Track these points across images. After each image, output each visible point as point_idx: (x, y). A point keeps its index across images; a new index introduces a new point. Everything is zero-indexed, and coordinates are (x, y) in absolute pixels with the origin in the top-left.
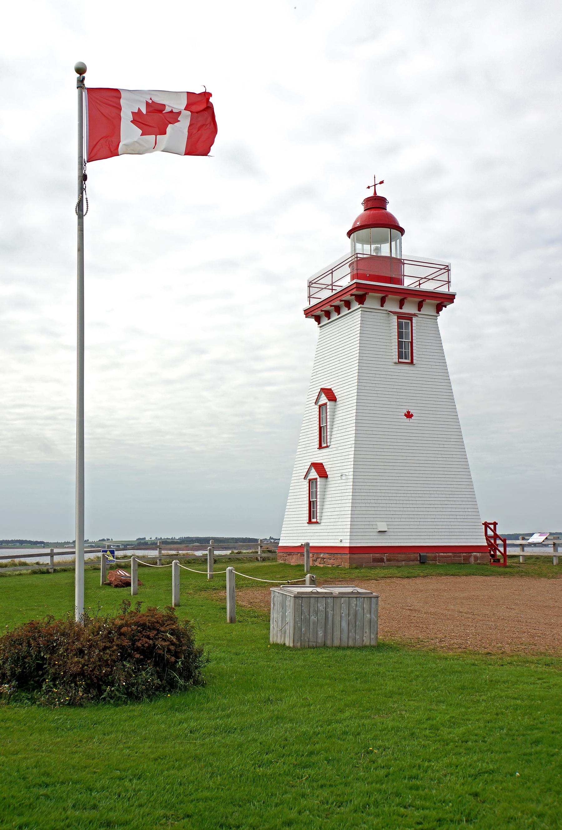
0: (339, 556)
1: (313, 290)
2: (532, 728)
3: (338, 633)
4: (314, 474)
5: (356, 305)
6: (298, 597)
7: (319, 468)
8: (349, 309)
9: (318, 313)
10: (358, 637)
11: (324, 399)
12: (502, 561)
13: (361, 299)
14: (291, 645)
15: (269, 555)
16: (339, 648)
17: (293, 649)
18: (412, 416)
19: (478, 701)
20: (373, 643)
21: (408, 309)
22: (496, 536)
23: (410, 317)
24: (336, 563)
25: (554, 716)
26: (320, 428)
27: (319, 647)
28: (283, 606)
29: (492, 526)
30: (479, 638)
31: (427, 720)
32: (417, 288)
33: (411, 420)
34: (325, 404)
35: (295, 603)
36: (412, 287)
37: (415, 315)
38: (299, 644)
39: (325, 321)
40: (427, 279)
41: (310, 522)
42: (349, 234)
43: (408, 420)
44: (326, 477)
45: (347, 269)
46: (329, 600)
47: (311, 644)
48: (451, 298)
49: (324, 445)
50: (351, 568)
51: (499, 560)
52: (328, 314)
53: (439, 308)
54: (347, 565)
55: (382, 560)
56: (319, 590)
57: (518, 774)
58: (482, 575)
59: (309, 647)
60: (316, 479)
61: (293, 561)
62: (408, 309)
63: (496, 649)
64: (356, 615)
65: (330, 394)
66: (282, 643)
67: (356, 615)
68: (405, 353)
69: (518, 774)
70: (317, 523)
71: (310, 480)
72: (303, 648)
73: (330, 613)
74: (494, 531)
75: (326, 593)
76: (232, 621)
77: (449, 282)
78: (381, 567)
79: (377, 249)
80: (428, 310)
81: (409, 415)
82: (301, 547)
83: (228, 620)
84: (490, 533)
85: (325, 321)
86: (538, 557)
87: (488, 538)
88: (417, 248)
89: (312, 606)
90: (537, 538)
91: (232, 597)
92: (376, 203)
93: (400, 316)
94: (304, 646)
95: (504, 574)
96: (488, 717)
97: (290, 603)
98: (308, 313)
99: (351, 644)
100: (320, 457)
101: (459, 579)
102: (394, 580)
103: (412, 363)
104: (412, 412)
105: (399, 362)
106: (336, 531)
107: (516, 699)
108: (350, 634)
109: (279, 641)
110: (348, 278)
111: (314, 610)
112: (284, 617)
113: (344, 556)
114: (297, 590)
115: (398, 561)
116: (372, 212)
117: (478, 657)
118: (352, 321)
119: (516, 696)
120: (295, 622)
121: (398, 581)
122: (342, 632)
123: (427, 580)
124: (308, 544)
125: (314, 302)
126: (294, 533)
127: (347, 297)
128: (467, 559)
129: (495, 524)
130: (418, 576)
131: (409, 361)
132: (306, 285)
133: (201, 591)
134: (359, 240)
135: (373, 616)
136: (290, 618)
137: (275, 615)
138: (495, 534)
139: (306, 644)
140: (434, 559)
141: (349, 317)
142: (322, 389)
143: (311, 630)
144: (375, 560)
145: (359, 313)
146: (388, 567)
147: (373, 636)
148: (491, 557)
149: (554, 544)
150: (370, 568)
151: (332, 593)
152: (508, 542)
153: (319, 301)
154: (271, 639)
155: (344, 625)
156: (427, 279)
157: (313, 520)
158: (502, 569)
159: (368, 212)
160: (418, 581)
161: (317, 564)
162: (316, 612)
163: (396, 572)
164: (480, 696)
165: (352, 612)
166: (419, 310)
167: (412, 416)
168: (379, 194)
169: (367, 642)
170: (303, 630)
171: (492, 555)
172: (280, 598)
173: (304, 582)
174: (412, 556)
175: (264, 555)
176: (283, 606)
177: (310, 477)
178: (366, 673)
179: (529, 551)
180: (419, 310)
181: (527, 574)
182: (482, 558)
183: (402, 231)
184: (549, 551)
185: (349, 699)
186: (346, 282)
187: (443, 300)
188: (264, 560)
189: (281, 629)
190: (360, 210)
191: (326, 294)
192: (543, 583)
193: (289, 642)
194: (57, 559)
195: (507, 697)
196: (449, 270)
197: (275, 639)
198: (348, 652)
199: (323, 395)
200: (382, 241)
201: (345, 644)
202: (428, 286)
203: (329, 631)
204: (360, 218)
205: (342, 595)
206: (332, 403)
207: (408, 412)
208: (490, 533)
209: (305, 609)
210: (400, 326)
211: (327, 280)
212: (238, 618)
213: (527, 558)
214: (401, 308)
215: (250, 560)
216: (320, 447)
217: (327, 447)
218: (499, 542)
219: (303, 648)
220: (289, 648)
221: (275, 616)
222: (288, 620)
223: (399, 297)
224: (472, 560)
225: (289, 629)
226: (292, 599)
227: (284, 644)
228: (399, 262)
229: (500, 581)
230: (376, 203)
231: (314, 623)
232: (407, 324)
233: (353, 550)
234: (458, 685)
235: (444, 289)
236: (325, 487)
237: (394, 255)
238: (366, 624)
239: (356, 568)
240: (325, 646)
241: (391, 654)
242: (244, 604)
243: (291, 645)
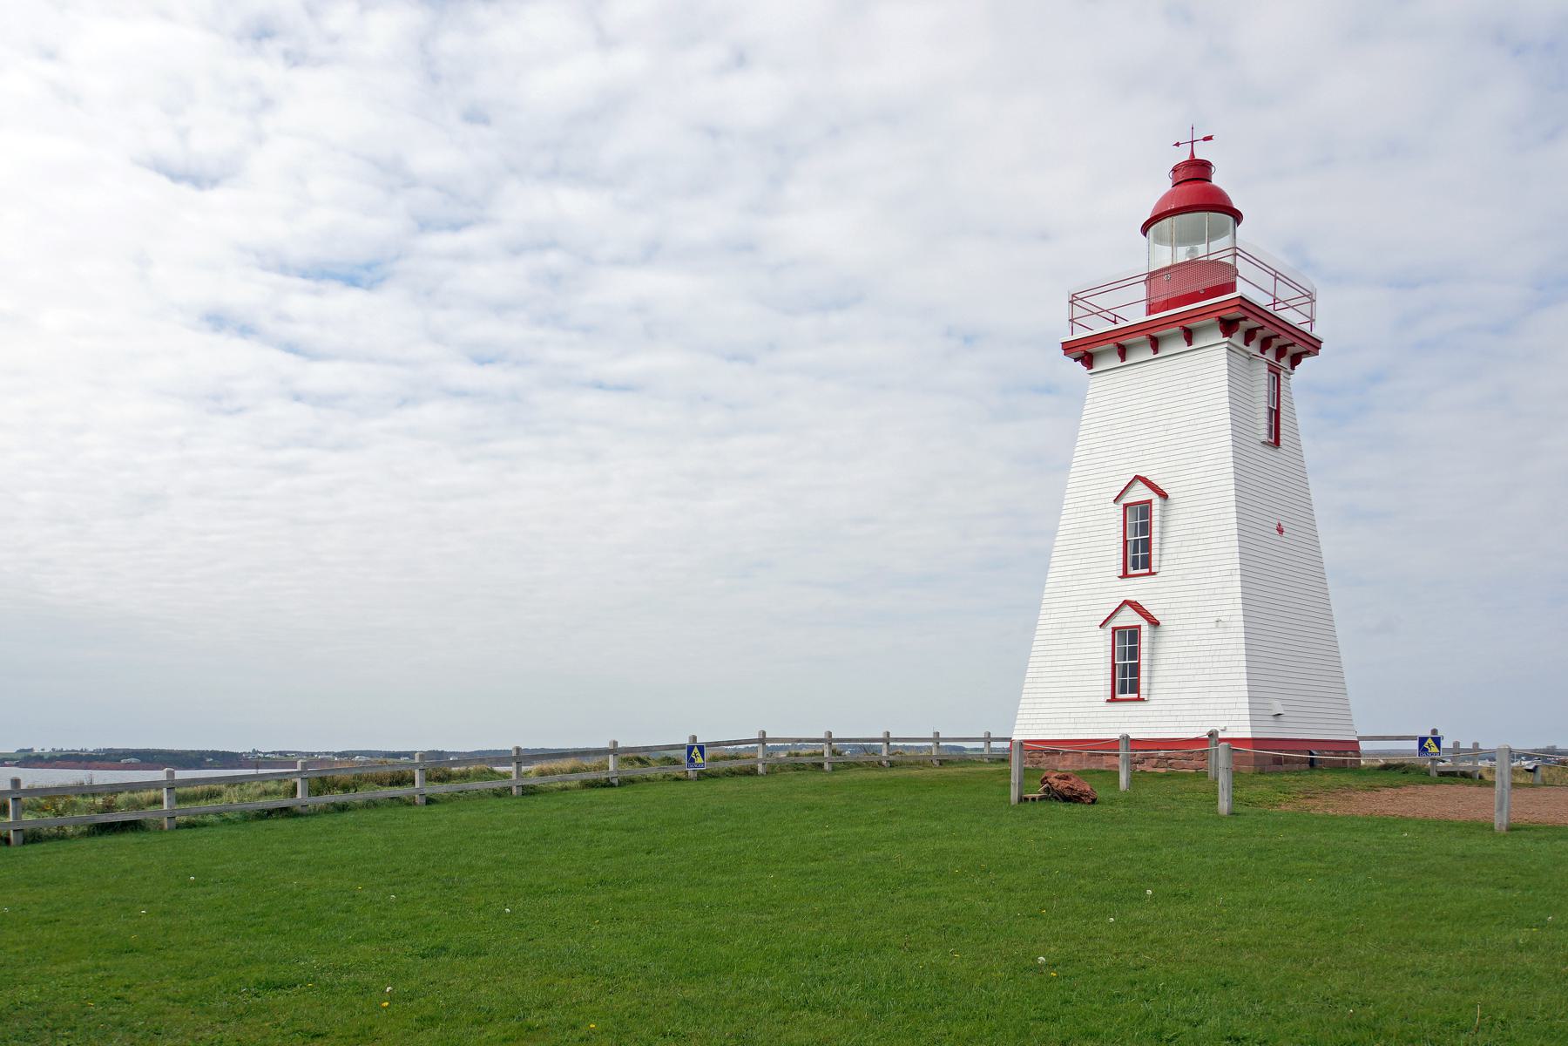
1: (1078, 312)
32: (1270, 309)
42: (1145, 228)
48: (1313, 346)
57: (1149, 892)
60: (1150, 502)
69: (1149, 892)
79: (1193, 251)
92: (1195, 172)
116: (1187, 187)
125: (1081, 333)
132: (1067, 299)
134: (1159, 239)
145: (1222, 352)
153: (1090, 333)
159: (1178, 188)
183: (1237, 216)
190: (1167, 185)
194: (994, 745)
204: (1167, 198)
230: (1195, 172)
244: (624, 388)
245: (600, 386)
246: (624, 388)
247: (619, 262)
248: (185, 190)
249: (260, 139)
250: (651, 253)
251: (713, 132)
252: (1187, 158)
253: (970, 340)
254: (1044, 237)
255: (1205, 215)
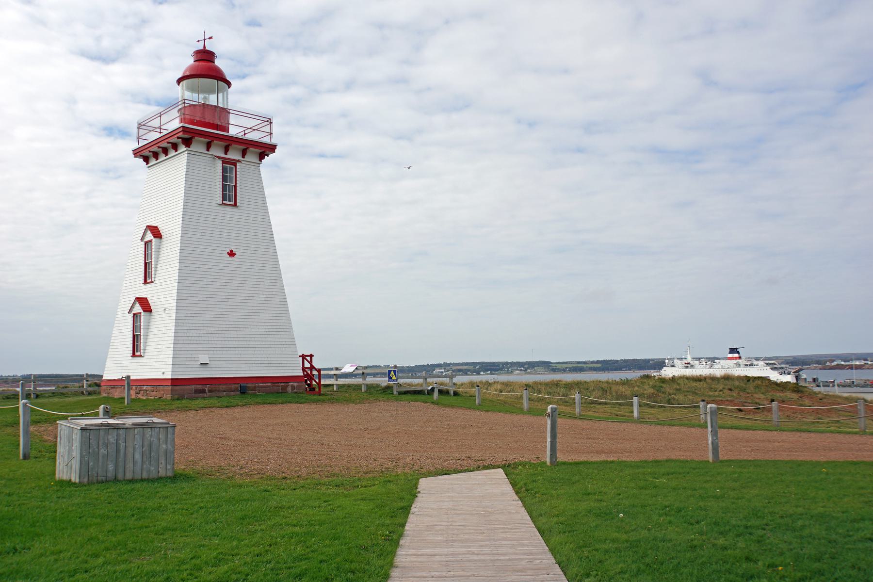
0: (161, 388)
1: (142, 132)
2: (299, 559)
3: (131, 465)
4: (138, 309)
5: (182, 148)
6: (85, 429)
7: (144, 303)
8: (176, 151)
9: (146, 153)
10: (152, 468)
11: (149, 236)
12: (317, 390)
13: (187, 142)
14: (77, 481)
15: (96, 388)
16: (132, 481)
17: (81, 484)
18: (234, 254)
19: (256, 532)
20: (169, 474)
21: (233, 155)
22: (312, 367)
23: (234, 163)
24: (158, 395)
25: (327, 542)
26: (146, 264)
27: (109, 481)
28: (70, 440)
29: (308, 358)
30: (279, 463)
31: (192, 558)
32: (243, 137)
33: (234, 259)
34: (151, 241)
35: (82, 436)
36: (240, 135)
37: (239, 161)
38: (86, 480)
39: (153, 161)
40: (253, 129)
41: (134, 355)
43: (230, 258)
44: (150, 311)
45: (175, 113)
46: (122, 432)
47: (100, 478)
48: (272, 148)
49: (149, 281)
50: (173, 399)
51: (314, 389)
52: (156, 155)
53: (262, 156)
54: (169, 397)
55: (203, 391)
56: (111, 421)
58: (297, 402)
59: (98, 482)
61: (116, 394)
62: (233, 155)
63: (293, 473)
64: (150, 446)
65: (156, 232)
66: (68, 479)
67: (150, 446)
68: (229, 195)
70: (140, 356)
71: (134, 315)
72: (90, 483)
73: (122, 445)
74: (311, 362)
75: (118, 424)
76: (26, 457)
77: (271, 134)
78: (204, 398)
80: (251, 157)
81: (231, 254)
82: (121, 380)
83: (21, 457)
84: (307, 365)
85: (153, 161)
86: (349, 386)
87: (304, 369)
88: (245, 105)
89: (101, 438)
90: (348, 369)
91: (26, 432)
92: (205, 56)
93: (225, 161)
94: (91, 480)
95: (316, 402)
96: (257, 550)
97: (77, 437)
98: (137, 153)
99: (145, 476)
100: (145, 292)
101: (275, 407)
102: (212, 410)
103: (235, 205)
104: (234, 251)
105: (224, 204)
106: (158, 364)
107: (294, 525)
108: (145, 466)
109: (65, 477)
110: (178, 120)
111: (104, 443)
112: (70, 451)
113: (166, 388)
114: (84, 422)
115: (219, 391)
116: (201, 63)
117: (273, 482)
118: (178, 164)
119: (295, 522)
120: (82, 456)
121: (217, 411)
122: (135, 462)
123: (245, 409)
124: (128, 377)
125: (143, 143)
126: (117, 365)
127: (174, 140)
128: (284, 390)
129: (311, 356)
130: (237, 405)
131: (232, 203)
132: (136, 126)
133: (7, 426)
135: (170, 447)
136: (76, 453)
137: (61, 449)
138: (311, 365)
139: (95, 480)
140: (254, 389)
141: (176, 159)
142: (148, 226)
143: (100, 464)
144: (196, 391)
145: (185, 155)
146: (210, 397)
147: (169, 467)
148: (307, 386)
149: (363, 373)
150: (191, 398)
151: (124, 424)
152: (322, 372)
154: (57, 476)
155: (138, 456)
156: (253, 129)
157: (137, 354)
158: (316, 397)
159: (197, 63)
160: (236, 410)
161: (140, 396)
162: (107, 446)
163: (216, 402)
164: (260, 525)
165: (146, 443)
166: (243, 157)
167: (234, 254)
168: (207, 48)
169: (162, 473)
170: (91, 464)
171: (308, 385)
172: (67, 432)
173: (97, 414)
174: (233, 386)
175: (90, 389)
176: (70, 440)
177: (134, 311)
178: (145, 508)
179: (341, 381)
180: (243, 157)
181: (338, 401)
182: (298, 387)
184: (359, 380)
185: (114, 539)
186: (176, 124)
187: (265, 150)
188: (90, 393)
189: (67, 465)
190: (190, 61)
191: (154, 136)
192: (351, 408)
193: (75, 478)
195: (287, 524)
196: (271, 123)
197: (61, 475)
198: (138, 485)
199: (149, 232)
200: (211, 92)
201: (138, 476)
202: (253, 136)
203: (121, 464)
204: (191, 68)
205: (135, 426)
206: (158, 240)
207: (231, 251)
208: (307, 365)
209: (93, 442)
210: (224, 170)
211: (156, 123)
212: (33, 453)
213: (340, 386)
214: (226, 153)
215: (75, 394)
216: (145, 282)
217: (152, 282)
218: (315, 372)
219: (90, 483)
220: (75, 483)
221: (62, 450)
222: (74, 454)
223: (224, 144)
224: (289, 389)
225: (76, 464)
226: (79, 432)
227: (70, 480)
228: (225, 112)
229: (312, 407)
230: (205, 56)
231: (103, 457)
232: (231, 169)
233: (174, 382)
234: (239, 514)
235: (266, 140)
236: (148, 322)
237: (220, 105)
238: (162, 454)
239: (178, 399)
240: (116, 480)
241: (184, 485)
242: (49, 438)
243: (77, 481)
244: (339, 156)
245: (322, 156)
246: (339, 156)
247: (332, 91)
248: (96, 64)
249: (139, 40)
250: (349, 86)
251: (381, 26)
252: (201, 48)
253: (532, 124)
254: (566, 71)
255: (196, 80)
